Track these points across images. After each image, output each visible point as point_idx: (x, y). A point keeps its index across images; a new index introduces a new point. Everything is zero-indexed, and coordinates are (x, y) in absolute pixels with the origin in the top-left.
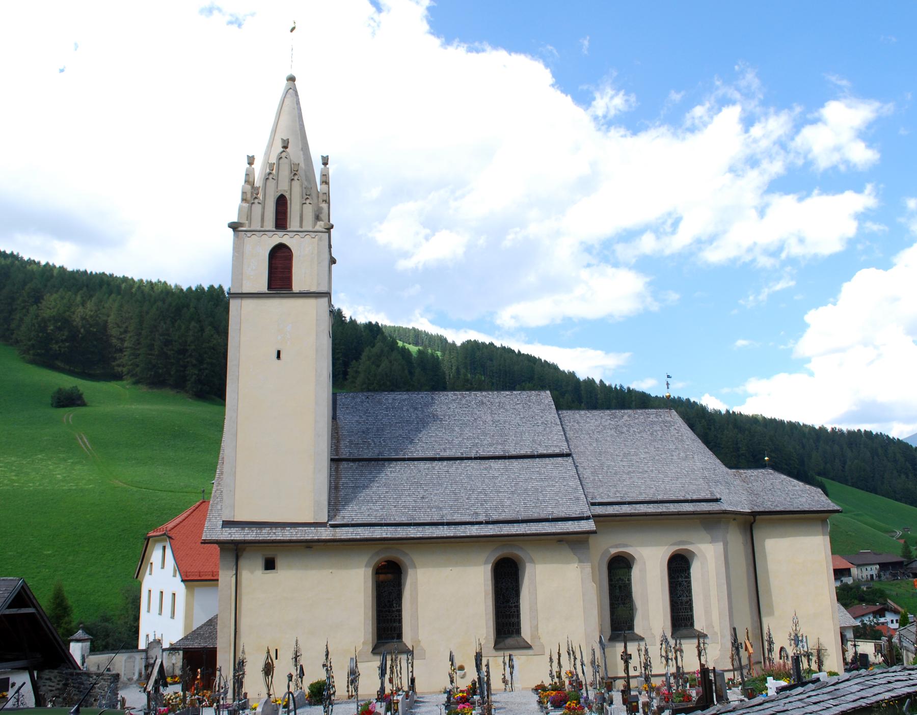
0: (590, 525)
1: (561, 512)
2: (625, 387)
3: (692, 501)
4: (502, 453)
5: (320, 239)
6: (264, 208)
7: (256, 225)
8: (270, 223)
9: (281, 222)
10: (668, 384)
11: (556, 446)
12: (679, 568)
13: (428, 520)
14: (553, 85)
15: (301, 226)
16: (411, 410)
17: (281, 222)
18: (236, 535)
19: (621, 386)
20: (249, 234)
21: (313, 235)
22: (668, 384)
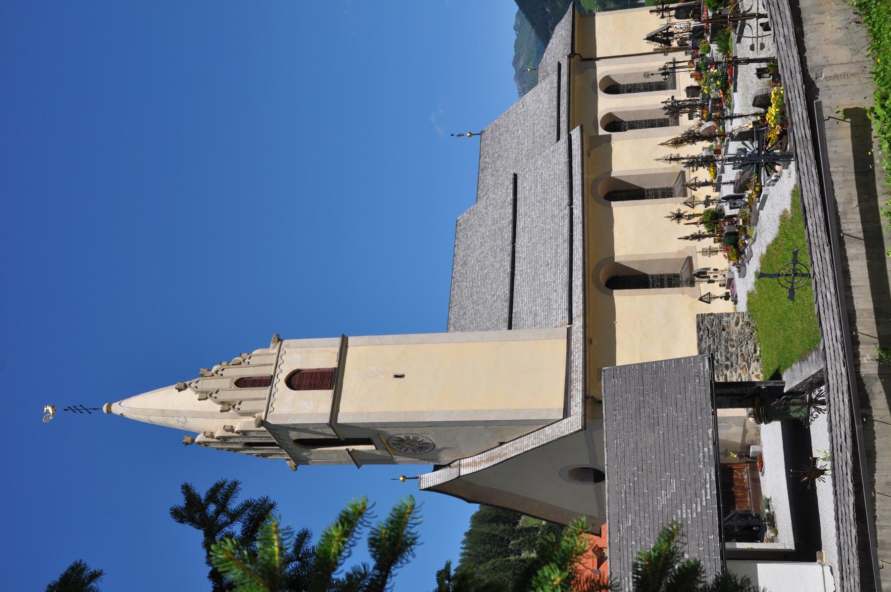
0: (576, 133)
1: (564, 158)
2: (464, 538)
3: (571, 203)
4: (511, 226)
5: (288, 346)
6: (246, 400)
7: (263, 405)
8: (264, 392)
9: (266, 382)
10: (459, 136)
11: (507, 189)
12: (613, 88)
13: (566, 245)
14: (95, 576)
15: (271, 365)
16: (466, 316)
17: (266, 382)
18: (577, 408)
19: (463, 542)
20: (270, 409)
21: (282, 352)
22: (459, 136)
